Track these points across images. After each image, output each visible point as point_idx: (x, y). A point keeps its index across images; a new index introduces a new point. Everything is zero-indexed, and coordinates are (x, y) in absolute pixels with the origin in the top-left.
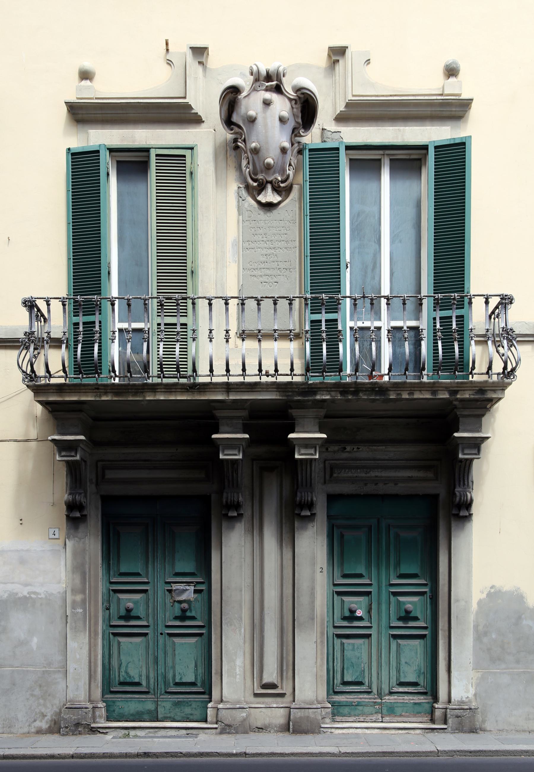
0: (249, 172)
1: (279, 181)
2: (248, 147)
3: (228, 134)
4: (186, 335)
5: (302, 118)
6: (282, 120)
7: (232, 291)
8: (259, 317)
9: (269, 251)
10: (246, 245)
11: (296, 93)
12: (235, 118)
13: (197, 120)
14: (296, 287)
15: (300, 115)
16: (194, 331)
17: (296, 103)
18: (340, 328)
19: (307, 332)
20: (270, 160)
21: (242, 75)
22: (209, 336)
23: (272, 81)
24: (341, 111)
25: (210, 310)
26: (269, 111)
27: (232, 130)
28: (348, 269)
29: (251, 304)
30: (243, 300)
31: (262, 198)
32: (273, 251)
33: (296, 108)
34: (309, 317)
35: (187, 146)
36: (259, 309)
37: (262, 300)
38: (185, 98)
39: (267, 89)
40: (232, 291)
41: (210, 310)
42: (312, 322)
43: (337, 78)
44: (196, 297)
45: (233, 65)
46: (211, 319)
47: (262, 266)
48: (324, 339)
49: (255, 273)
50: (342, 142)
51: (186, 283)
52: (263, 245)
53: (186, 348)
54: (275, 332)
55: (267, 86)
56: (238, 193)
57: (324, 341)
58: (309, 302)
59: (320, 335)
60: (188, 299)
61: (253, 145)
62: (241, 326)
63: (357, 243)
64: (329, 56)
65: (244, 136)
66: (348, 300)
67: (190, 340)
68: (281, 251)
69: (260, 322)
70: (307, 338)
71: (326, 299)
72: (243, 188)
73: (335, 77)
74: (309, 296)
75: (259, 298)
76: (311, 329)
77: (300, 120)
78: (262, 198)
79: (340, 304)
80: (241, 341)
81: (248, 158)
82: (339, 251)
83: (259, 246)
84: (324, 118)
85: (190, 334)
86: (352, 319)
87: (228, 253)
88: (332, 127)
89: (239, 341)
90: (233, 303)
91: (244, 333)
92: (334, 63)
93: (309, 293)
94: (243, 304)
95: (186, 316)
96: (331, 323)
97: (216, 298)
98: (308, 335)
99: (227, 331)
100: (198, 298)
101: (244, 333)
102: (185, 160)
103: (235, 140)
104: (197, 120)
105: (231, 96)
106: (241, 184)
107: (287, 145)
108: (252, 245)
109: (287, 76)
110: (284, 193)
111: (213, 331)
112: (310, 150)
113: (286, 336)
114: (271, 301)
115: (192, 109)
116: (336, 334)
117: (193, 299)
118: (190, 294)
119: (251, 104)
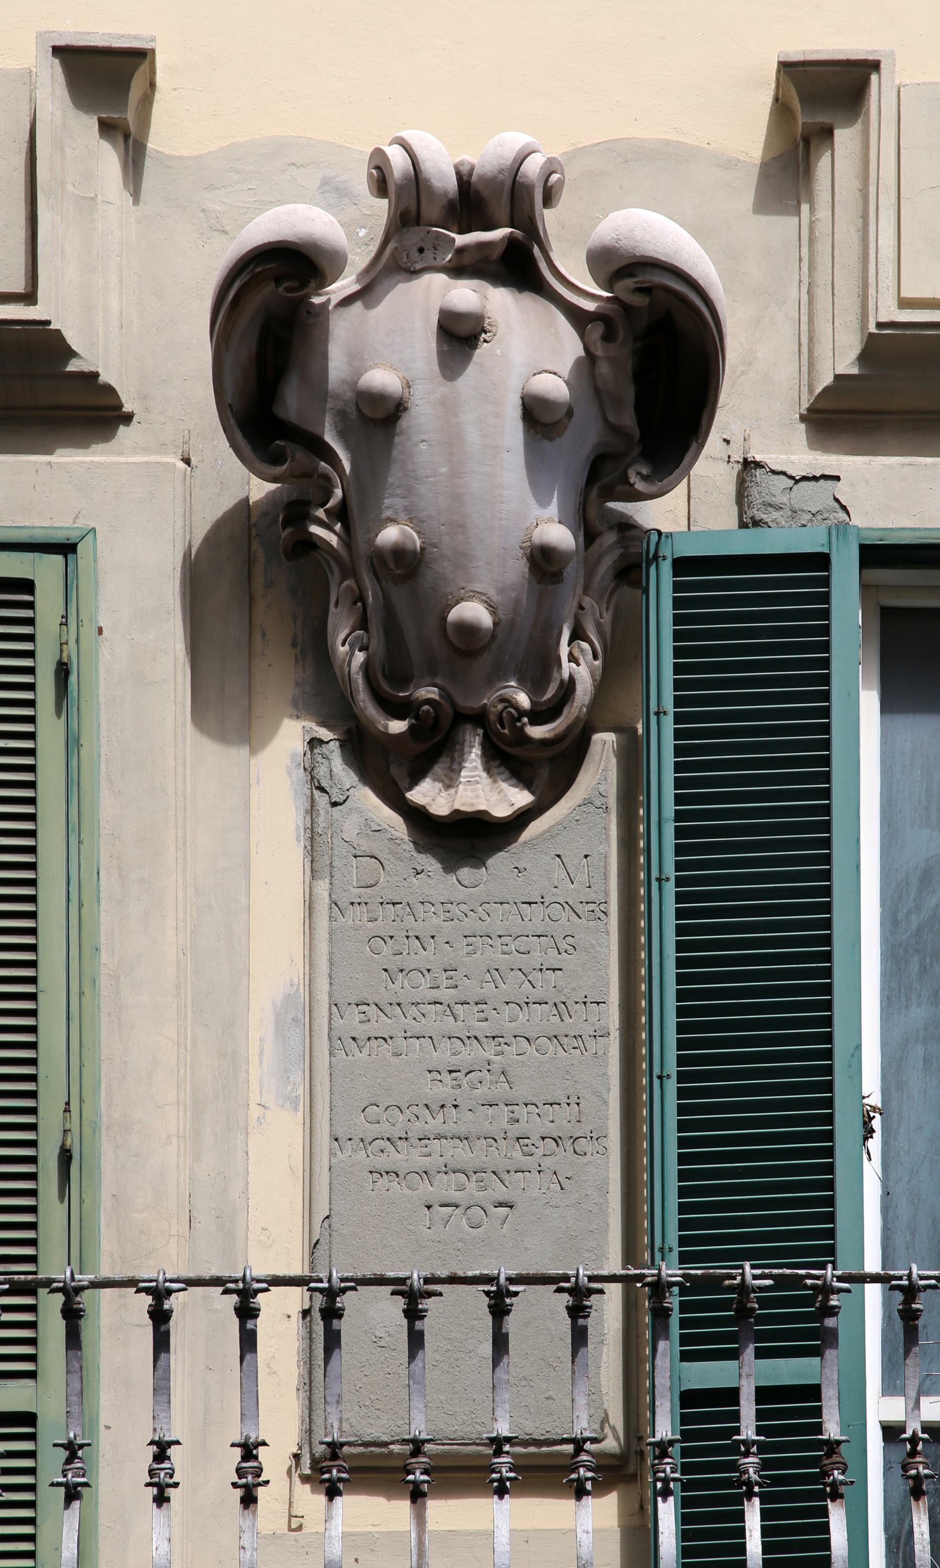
0: (367, 667)
1: (522, 713)
2: (362, 547)
3: (255, 480)
4: (31, 1471)
5: (640, 408)
6: (537, 416)
7: (274, 1245)
8: (415, 1381)
9: (470, 1054)
10: (352, 1021)
11: (608, 284)
12: (292, 404)
13: (91, 412)
14: (606, 1230)
15: (629, 394)
16: (72, 1450)
17: (608, 337)
18: (832, 1429)
19: (663, 1448)
20: (473, 611)
21: (332, 192)
22: (152, 1472)
23: (482, 223)
24: (837, 377)
25: (161, 1343)
26: (471, 370)
27: (276, 459)
28: (875, 1144)
29: (374, 1316)
30: (331, 1294)
31: (429, 795)
32: (488, 1052)
33: (612, 360)
34: (671, 1373)
35: (40, 536)
36: (416, 1341)
37: (430, 1294)
38: (29, 297)
39: (464, 267)
40: (274, 1245)
41: (161, 1343)
42: (689, 1398)
43: (823, 213)
44: (84, 1278)
45: (286, 123)
46: (161, 1388)
47: (434, 1124)
48: (749, 1484)
49: (394, 1158)
50: (842, 529)
51: (33, 1210)
52: (436, 1021)
53: (31, 1538)
54: (498, 1452)
55: (461, 251)
56: (310, 771)
57: (750, 1495)
58: (673, 1301)
59: (733, 1466)
60: (43, 1292)
61: (390, 535)
62: (319, 1421)
63: (919, 1014)
64: (781, 108)
65: (338, 492)
66: (873, 1293)
67: (50, 1498)
68: (531, 1050)
69: (418, 1403)
70: (666, 1481)
71: (762, 1289)
72: (334, 746)
73: (812, 210)
74: (671, 1271)
75: (417, 1282)
76: (686, 1436)
77: (629, 420)
78: (429, 795)
79: (833, 1312)
80: (322, 1499)
81: (362, 598)
82: (829, 1054)
83: (417, 1028)
84: (758, 405)
85: (51, 1465)
86: (890, 1387)
87: (254, 1059)
88: (794, 453)
89: (311, 1501)
90: (280, 1313)
91: (334, 1457)
92: (807, 141)
93: (675, 1256)
94: (331, 1313)
95: (32, 1375)
96: (791, 1407)
97: (192, 1283)
98: (669, 1468)
99: (249, 1450)
100: (97, 1285)
101: (334, 1457)
102: (30, 605)
103: (295, 512)
104: (91, 412)
105: (271, 305)
106: (322, 724)
107: (560, 535)
108: (381, 1024)
109: (565, 200)
110: (544, 773)
111: (173, 1451)
112: (682, 565)
113: (548, 1470)
114: (476, 1300)
115: (71, 354)
116: (814, 1462)
117: (70, 1292)
118: (54, 1266)
119: (377, 343)
